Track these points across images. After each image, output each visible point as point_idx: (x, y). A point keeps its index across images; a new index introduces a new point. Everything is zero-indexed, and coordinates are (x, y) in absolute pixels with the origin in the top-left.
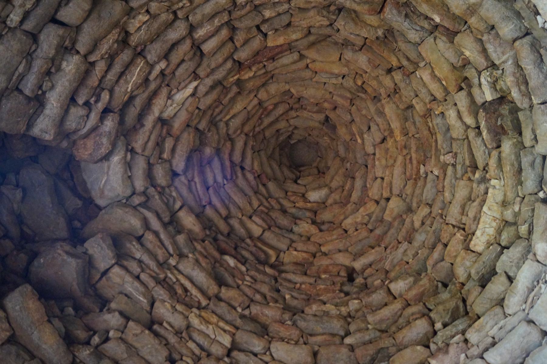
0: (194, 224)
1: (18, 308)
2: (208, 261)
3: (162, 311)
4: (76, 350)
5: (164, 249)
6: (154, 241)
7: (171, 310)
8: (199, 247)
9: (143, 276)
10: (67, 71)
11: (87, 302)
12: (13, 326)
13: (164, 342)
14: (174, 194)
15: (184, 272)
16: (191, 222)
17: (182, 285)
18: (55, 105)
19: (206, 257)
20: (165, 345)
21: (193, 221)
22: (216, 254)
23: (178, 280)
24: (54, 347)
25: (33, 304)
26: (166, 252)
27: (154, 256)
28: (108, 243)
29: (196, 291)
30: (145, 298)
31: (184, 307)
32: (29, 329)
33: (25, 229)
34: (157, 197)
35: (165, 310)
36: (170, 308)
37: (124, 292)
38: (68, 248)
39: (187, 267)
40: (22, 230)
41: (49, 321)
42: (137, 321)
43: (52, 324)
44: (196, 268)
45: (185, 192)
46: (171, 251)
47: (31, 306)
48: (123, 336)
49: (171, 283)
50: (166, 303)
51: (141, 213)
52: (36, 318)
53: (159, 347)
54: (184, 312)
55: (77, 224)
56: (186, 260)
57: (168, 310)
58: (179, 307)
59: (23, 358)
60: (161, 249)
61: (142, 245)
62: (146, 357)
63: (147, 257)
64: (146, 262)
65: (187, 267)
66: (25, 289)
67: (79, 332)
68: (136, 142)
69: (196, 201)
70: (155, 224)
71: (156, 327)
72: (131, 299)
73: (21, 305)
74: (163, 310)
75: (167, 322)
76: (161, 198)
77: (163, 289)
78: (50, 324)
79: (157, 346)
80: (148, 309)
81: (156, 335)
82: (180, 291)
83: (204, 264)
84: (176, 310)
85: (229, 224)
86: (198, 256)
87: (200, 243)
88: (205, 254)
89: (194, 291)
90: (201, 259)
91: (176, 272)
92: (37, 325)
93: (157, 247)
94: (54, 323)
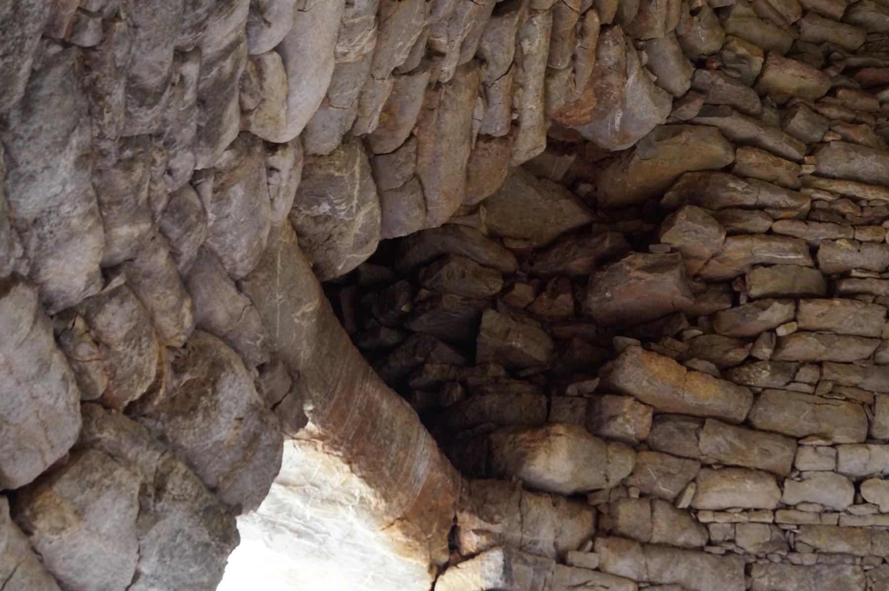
0: (802, 77)
1: (645, 383)
2: (864, 126)
3: (839, 258)
4: (745, 378)
5: (783, 161)
6: (762, 161)
7: (854, 249)
8: (834, 113)
9: (778, 227)
10: (535, 52)
11: (708, 305)
12: (649, 403)
13: (870, 299)
14: (742, 51)
15: (835, 174)
16: (793, 76)
17: (843, 196)
18: (534, 107)
19: (855, 123)
20: (874, 302)
21: (797, 73)
22: (867, 102)
23: (832, 193)
24: (720, 395)
25: (657, 364)
26: (789, 163)
27: (771, 183)
28: (700, 218)
29: (874, 192)
30: (798, 253)
31: (870, 230)
32: (676, 396)
33: (514, 245)
34: (720, 81)
35: (844, 255)
36: (849, 246)
37: (759, 261)
38: (640, 260)
39: (835, 161)
40: (513, 251)
41: (690, 369)
42: (809, 296)
43: (695, 370)
44: (853, 154)
45: (756, 31)
46: (797, 155)
47: (657, 370)
48: (801, 325)
49: (826, 206)
50: (838, 242)
51: (707, 125)
52: (674, 379)
53: (867, 311)
54: (876, 238)
55: (585, 188)
56: (826, 151)
57: (848, 250)
58: (864, 235)
59: (691, 430)
60: (781, 164)
61: (744, 177)
62: (852, 332)
63: (768, 194)
64: (770, 202)
65: (835, 161)
66: (635, 356)
67: (732, 354)
68: (652, 29)
69: (779, 27)
70: (742, 128)
71: (845, 286)
72: (774, 264)
73: (646, 378)
74: (840, 254)
75: (856, 269)
76: (729, 79)
77: (821, 225)
78: (692, 372)
79: (863, 312)
80: (810, 262)
81: (851, 296)
82: (846, 208)
83: (861, 139)
84: (861, 242)
85: (856, 24)
86: (843, 131)
87: (830, 105)
88: (851, 116)
89: (870, 194)
90: (851, 133)
91: (822, 182)
92: (682, 386)
93: (772, 167)
94: (696, 367)
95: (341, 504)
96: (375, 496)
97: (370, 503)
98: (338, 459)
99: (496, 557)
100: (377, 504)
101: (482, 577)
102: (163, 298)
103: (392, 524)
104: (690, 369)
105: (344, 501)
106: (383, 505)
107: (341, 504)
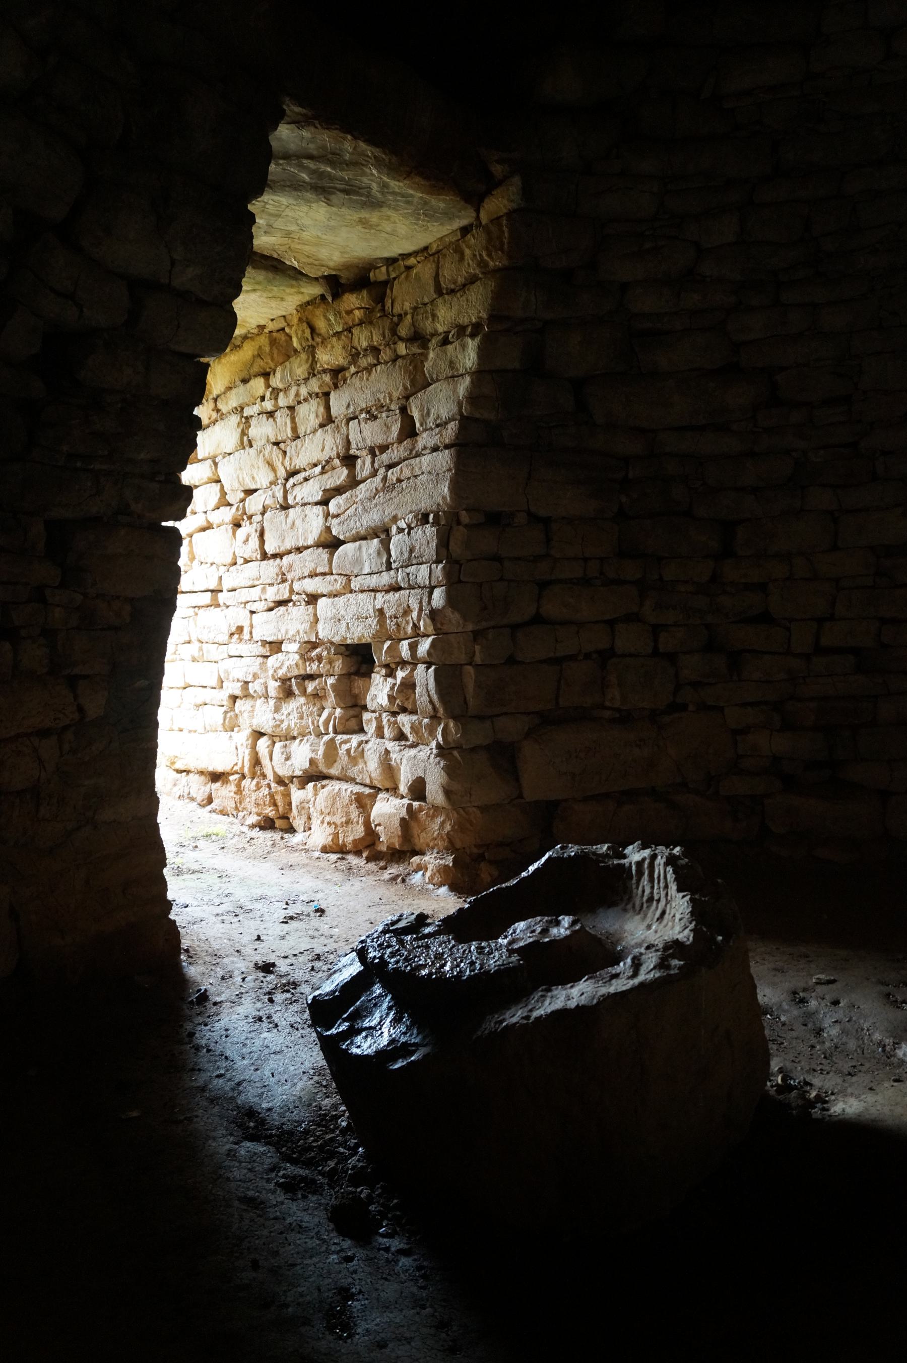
78: (231, 701)
95: (363, 165)
96: (385, 154)
97: (384, 160)
98: (336, 131)
99: (517, 180)
100: (390, 160)
101: (508, 200)
102: (339, 944)
103: (411, 173)
104: (232, 634)
105: (364, 162)
106: (394, 159)
107: (363, 165)
